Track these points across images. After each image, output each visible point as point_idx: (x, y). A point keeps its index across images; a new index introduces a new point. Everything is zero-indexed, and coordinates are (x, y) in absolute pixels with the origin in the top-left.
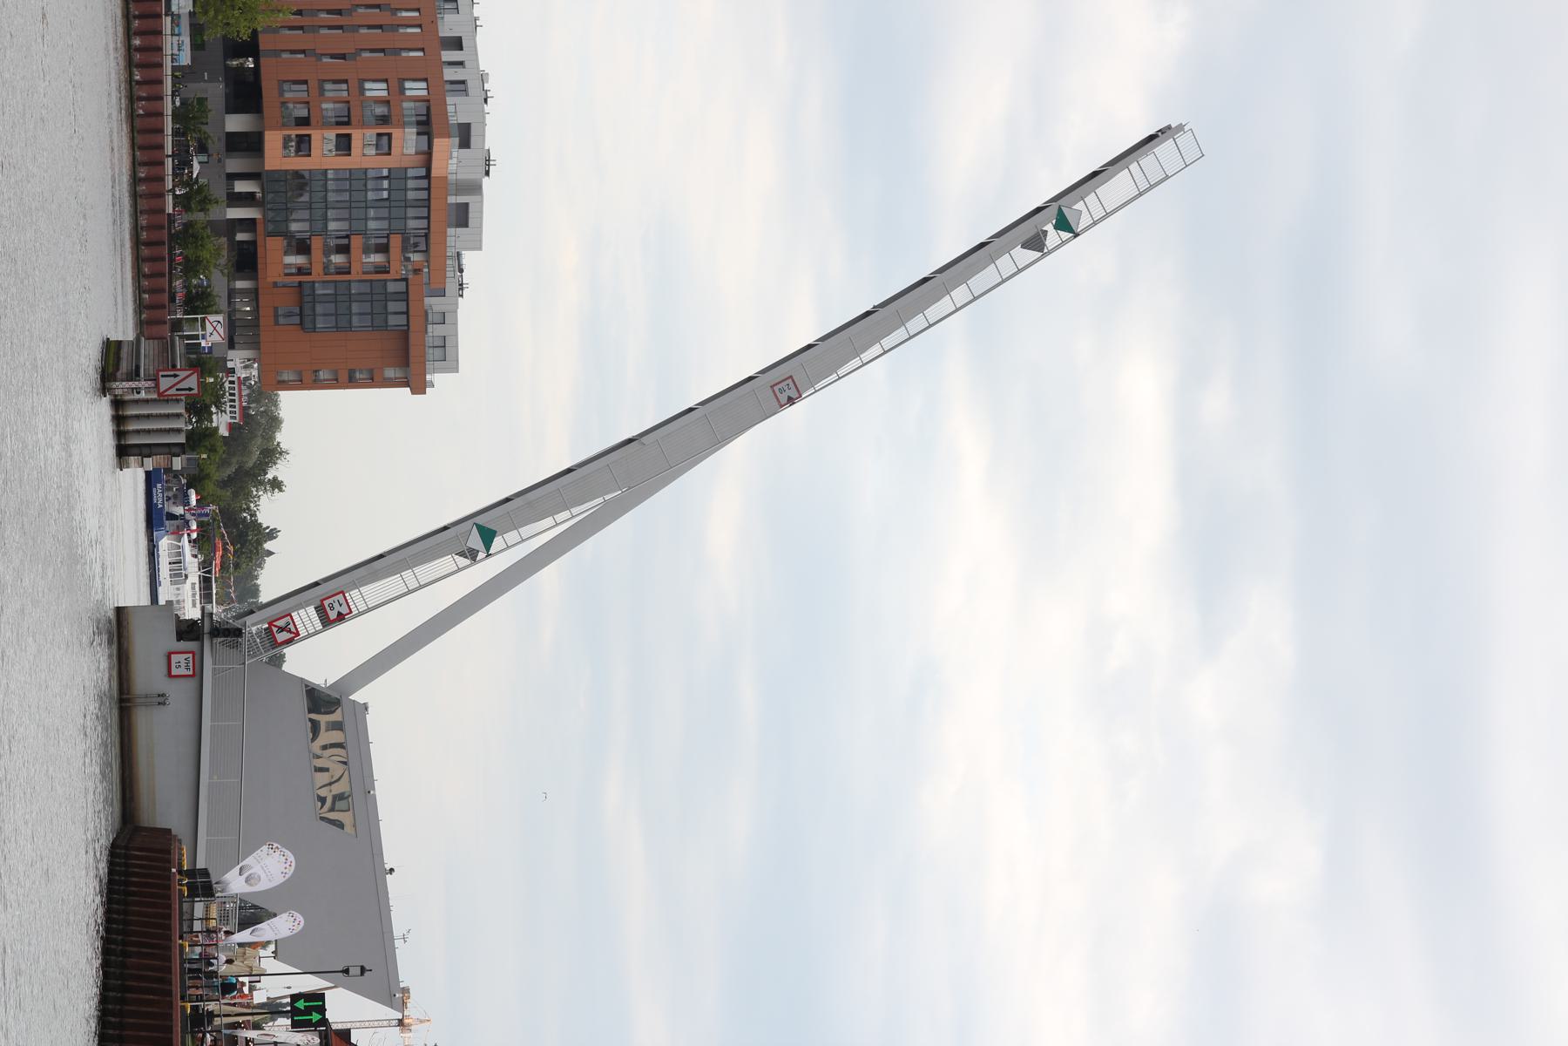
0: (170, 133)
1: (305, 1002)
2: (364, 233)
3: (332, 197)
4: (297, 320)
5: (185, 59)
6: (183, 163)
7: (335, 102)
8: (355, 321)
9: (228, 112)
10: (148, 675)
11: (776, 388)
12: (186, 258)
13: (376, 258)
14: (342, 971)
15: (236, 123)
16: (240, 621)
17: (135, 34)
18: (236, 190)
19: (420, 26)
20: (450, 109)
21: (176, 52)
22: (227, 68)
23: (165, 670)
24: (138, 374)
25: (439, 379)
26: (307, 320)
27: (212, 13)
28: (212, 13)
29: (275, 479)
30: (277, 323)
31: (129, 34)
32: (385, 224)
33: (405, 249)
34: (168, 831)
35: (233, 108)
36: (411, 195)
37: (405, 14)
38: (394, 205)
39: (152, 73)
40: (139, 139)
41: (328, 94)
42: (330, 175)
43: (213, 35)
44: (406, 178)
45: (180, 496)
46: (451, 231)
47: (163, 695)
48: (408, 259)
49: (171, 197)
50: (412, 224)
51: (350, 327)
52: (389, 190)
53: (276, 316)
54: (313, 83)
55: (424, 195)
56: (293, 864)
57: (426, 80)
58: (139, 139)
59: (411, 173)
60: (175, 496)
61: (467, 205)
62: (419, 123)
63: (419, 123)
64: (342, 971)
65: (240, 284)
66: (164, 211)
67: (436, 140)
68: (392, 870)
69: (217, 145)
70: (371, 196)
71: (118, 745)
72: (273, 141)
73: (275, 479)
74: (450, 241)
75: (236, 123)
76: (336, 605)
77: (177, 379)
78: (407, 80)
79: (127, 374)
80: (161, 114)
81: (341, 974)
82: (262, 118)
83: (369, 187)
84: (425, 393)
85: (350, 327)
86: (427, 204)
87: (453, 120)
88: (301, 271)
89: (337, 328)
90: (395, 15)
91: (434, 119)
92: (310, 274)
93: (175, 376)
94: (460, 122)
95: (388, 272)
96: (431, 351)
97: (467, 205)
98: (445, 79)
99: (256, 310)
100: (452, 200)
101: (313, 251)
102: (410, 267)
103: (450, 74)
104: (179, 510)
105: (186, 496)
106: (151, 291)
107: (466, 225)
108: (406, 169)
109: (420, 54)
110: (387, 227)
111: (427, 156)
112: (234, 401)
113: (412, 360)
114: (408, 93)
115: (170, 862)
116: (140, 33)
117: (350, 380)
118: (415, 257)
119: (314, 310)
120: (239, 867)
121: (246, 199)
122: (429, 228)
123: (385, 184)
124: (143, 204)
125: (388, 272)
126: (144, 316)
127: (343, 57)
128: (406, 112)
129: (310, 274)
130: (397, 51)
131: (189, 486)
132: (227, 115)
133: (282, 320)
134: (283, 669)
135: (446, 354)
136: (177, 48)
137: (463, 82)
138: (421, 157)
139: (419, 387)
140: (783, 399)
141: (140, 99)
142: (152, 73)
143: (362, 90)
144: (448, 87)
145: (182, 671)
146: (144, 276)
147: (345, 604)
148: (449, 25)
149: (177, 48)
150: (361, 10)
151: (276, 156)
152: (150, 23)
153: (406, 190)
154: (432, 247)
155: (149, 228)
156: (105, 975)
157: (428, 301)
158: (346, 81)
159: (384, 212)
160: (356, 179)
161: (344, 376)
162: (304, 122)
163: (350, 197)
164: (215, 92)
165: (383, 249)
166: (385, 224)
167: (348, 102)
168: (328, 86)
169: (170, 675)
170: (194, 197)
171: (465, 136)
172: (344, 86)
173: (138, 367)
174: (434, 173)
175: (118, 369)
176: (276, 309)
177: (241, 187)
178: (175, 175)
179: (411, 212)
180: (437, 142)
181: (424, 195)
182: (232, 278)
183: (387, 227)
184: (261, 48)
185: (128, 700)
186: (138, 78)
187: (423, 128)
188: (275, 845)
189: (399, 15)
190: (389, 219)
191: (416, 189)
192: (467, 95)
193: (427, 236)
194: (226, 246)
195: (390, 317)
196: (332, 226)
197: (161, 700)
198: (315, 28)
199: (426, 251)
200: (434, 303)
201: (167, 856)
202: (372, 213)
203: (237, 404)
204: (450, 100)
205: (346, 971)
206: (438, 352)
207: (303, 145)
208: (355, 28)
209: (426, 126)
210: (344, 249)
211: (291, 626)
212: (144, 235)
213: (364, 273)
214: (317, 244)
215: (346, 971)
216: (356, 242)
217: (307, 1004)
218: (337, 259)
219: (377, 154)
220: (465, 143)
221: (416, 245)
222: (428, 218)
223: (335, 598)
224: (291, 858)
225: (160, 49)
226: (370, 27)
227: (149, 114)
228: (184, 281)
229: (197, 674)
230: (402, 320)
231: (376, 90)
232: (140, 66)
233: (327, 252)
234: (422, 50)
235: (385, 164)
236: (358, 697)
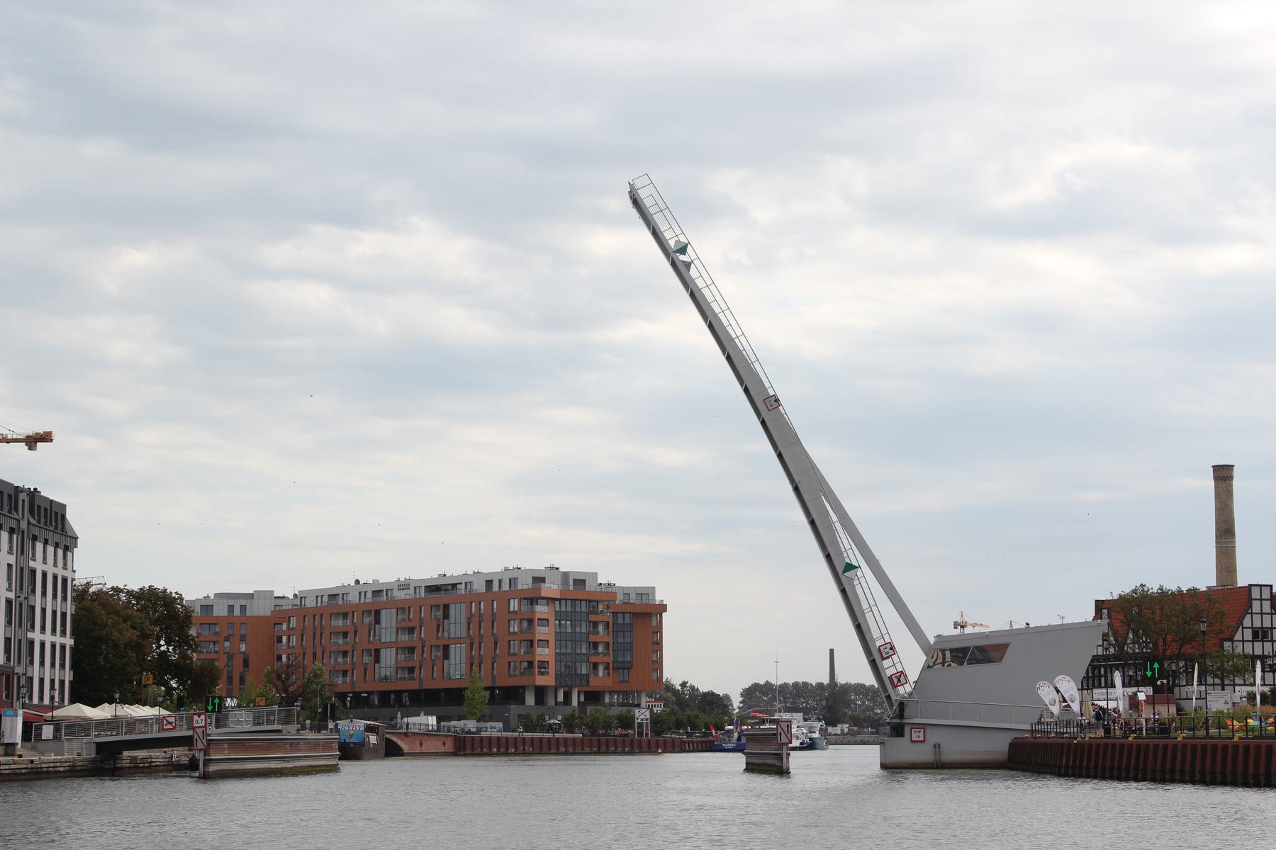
0: (542, 734)
2: (588, 634)
3: (569, 651)
4: (626, 671)
5: (500, 725)
6: (551, 728)
7: (521, 648)
8: (628, 640)
9: (524, 704)
10: (923, 753)
11: (770, 408)
12: (603, 727)
13: (601, 628)
15: (530, 700)
16: (894, 702)
17: (490, 750)
18: (562, 700)
19: (480, 602)
20: (525, 587)
21: (495, 730)
22: (351, 707)
23: (921, 744)
24: (779, 754)
25: (659, 597)
26: (627, 665)
27: (475, 710)
28: (475, 710)
29: (681, 685)
30: (628, 682)
31: (490, 754)
33: (596, 613)
34: (1011, 745)
35: (522, 701)
36: (569, 609)
37: (473, 610)
38: (573, 617)
39: (511, 742)
40: (545, 750)
41: (516, 651)
42: (558, 651)
43: (487, 710)
44: (560, 611)
45: (728, 734)
46: (588, 589)
47: (935, 745)
48: (602, 612)
49: (524, 734)
50: (584, 609)
51: (631, 643)
52: (566, 620)
53: (624, 682)
54: (510, 659)
55: (569, 602)
56: (1064, 676)
57: (509, 600)
58: (545, 750)
59: (558, 609)
60: (728, 737)
61: (574, 580)
62: (532, 604)
63: (532, 604)
65: (607, 700)
66: (582, 739)
67: (542, 595)
68: (1027, 624)
69: (541, 709)
70: (569, 630)
71: (981, 771)
72: (541, 681)
73: (681, 685)
74: (593, 589)
75: (530, 700)
76: (886, 650)
77: (782, 733)
78: (509, 609)
79: (778, 760)
80: (532, 738)
82: (528, 686)
83: (564, 631)
84: (666, 605)
85: (631, 643)
86: (573, 601)
87: (531, 586)
88: (607, 668)
89: (631, 650)
90: (473, 615)
91: (530, 596)
92: (608, 663)
93: (780, 734)
94: (531, 582)
95: (608, 622)
96: (644, 601)
97: (574, 580)
98: (498, 590)
99: (617, 692)
100: (571, 588)
101: (597, 661)
102: (606, 611)
103: (506, 587)
104: (736, 735)
105: (729, 731)
106: (624, 746)
107: (585, 580)
108: (555, 611)
109: (495, 602)
111: (550, 600)
112: (652, 705)
113: (649, 611)
114: (516, 609)
115: (1070, 744)
116: (490, 748)
117: (658, 645)
118: (600, 608)
119: (621, 662)
120: (1049, 706)
121: (567, 696)
122: (586, 600)
123: (563, 622)
124: (579, 749)
125: (608, 622)
126: (637, 751)
127: (496, 643)
128: (526, 611)
129: (608, 663)
130: (481, 615)
131: (722, 728)
132: (526, 704)
133: (626, 679)
135: (646, 593)
136: (494, 729)
137: (510, 580)
138: (550, 603)
139: (663, 608)
141: (524, 749)
142: (511, 742)
143: (514, 633)
144: (513, 588)
145: (921, 735)
146: (616, 749)
147: (885, 646)
148: (479, 587)
149: (494, 729)
150: (323, 642)
151: (547, 680)
152: (485, 743)
153: (566, 612)
154: (595, 599)
155: (591, 746)
156: (1144, 779)
157: (617, 602)
158: (509, 642)
159: (578, 623)
160: (560, 637)
161: (655, 647)
162: (531, 664)
163: (1257, 614)
164: (514, 710)
165: (595, 624)
166: (584, 624)
167: (521, 641)
168: (512, 651)
169: (922, 742)
170: (569, 725)
171: (539, 580)
172: (512, 642)
173: (775, 754)
174: (559, 597)
175: (775, 765)
176: (621, 682)
177: (561, 698)
178: (513, 731)
179: (578, 609)
180: (543, 595)
181: (583, 603)
182: (603, 704)
184: (417, 688)
185: (937, 764)
186: (513, 750)
187: (534, 603)
188: (1038, 686)
189: (473, 613)
192: (517, 578)
193: (590, 601)
194: (595, 707)
195: (625, 622)
196: (584, 651)
197: (937, 746)
198: (481, 657)
199: (597, 602)
200: (620, 598)
201: (1151, 748)
202: (578, 630)
203: (654, 704)
204: (520, 587)
206: (644, 598)
207: (543, 665)
208: (481, 636)
209: (533, 601)
210: (595, 645)
211: (897, 675)
212: (595, 749)
213: (608, 634)
214: (593, 659)
216: (593, 638)
218: (601, 649)
219: (548, 626)
220: (543, 580)
221: (594, 607)
222: (581, 600)
223: (882, 651)
224: (1060, 677)
225: (499, 738)
226: (480, 628)
227: (532, 745)
229: (923, 726)
230: (627, 616)
231: (515, 627)
232: (507, 748)
233: (598, 654)
234: (493, 601)
235: (553, 622)
236: (932, 641)
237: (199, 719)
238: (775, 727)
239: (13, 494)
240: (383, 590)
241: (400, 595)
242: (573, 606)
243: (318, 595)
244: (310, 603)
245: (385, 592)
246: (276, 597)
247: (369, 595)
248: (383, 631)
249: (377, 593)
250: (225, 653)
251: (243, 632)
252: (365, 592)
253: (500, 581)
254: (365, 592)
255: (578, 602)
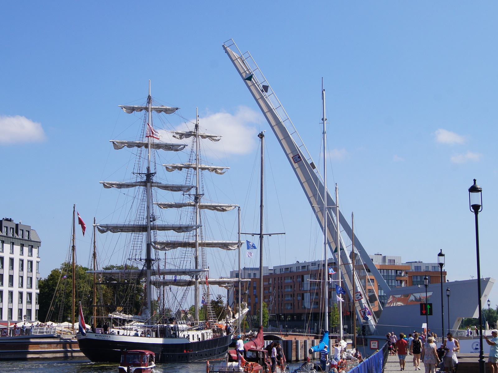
1: (423, 310)
14: (476, 213)
32: (393, 281)
55: (385, 271)
64: (476, 213)
81: (479, 215)
110: (394, 281)
134: (423, 324)
140: (299, 159)
154: (401, 269)
159: (390, 281)
166: (393, 281)
179: (390, 274)
181: (385, 271)
183: (394, 281)
190: (392, 280)
191: (384, 273)
205: (476, 208)
215: (476, 208)
217: (424, 310)
222: (384, 270)
228: (422, 359)
237: (18, 331)
238: (140, 355)
239: (15, 227)
240: (305, 266)
241: (311, 268)
242: (388, 272)
243: (281, 268)
244: (278, 272)
245: (306, 266)
246: (269, 270)
247: (300, 268)
248: (305, 285)
249: (303, 267)
250: (254, 295)
251: (255, 285)
252: (282, 269)
253: (299, 267)
254: (282, 269)
255: (390, 271)
